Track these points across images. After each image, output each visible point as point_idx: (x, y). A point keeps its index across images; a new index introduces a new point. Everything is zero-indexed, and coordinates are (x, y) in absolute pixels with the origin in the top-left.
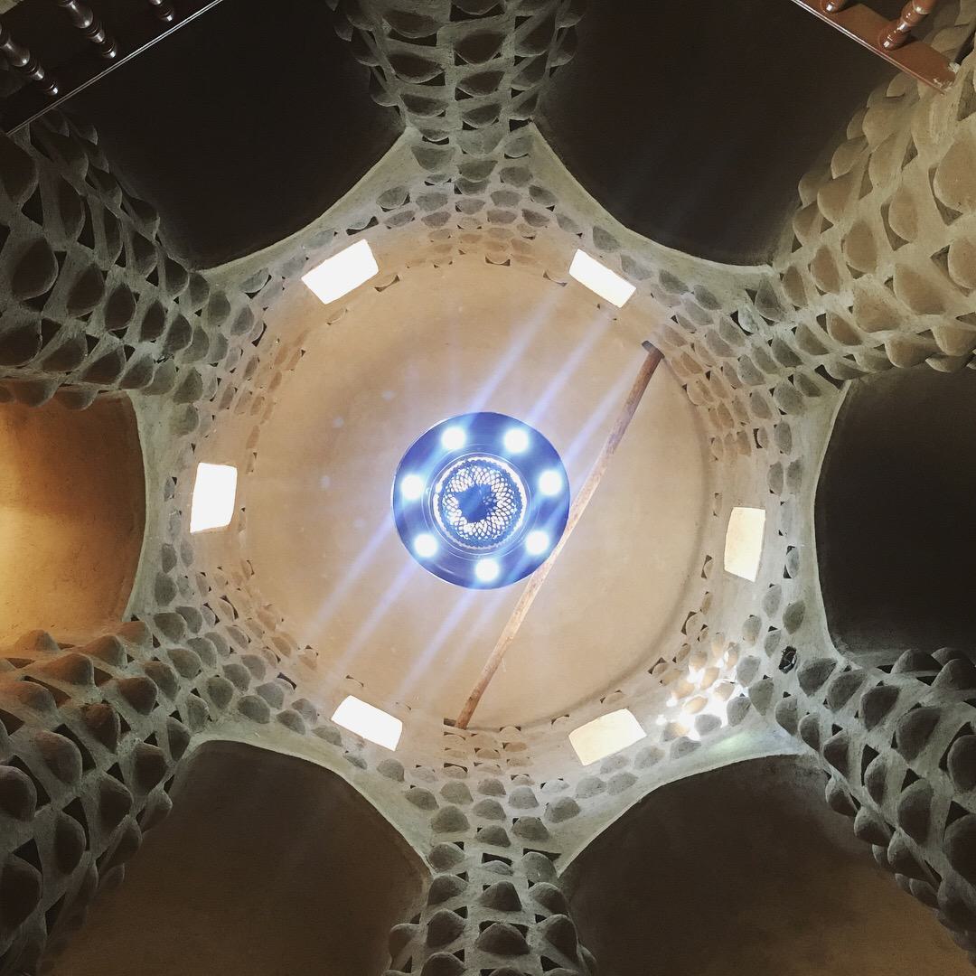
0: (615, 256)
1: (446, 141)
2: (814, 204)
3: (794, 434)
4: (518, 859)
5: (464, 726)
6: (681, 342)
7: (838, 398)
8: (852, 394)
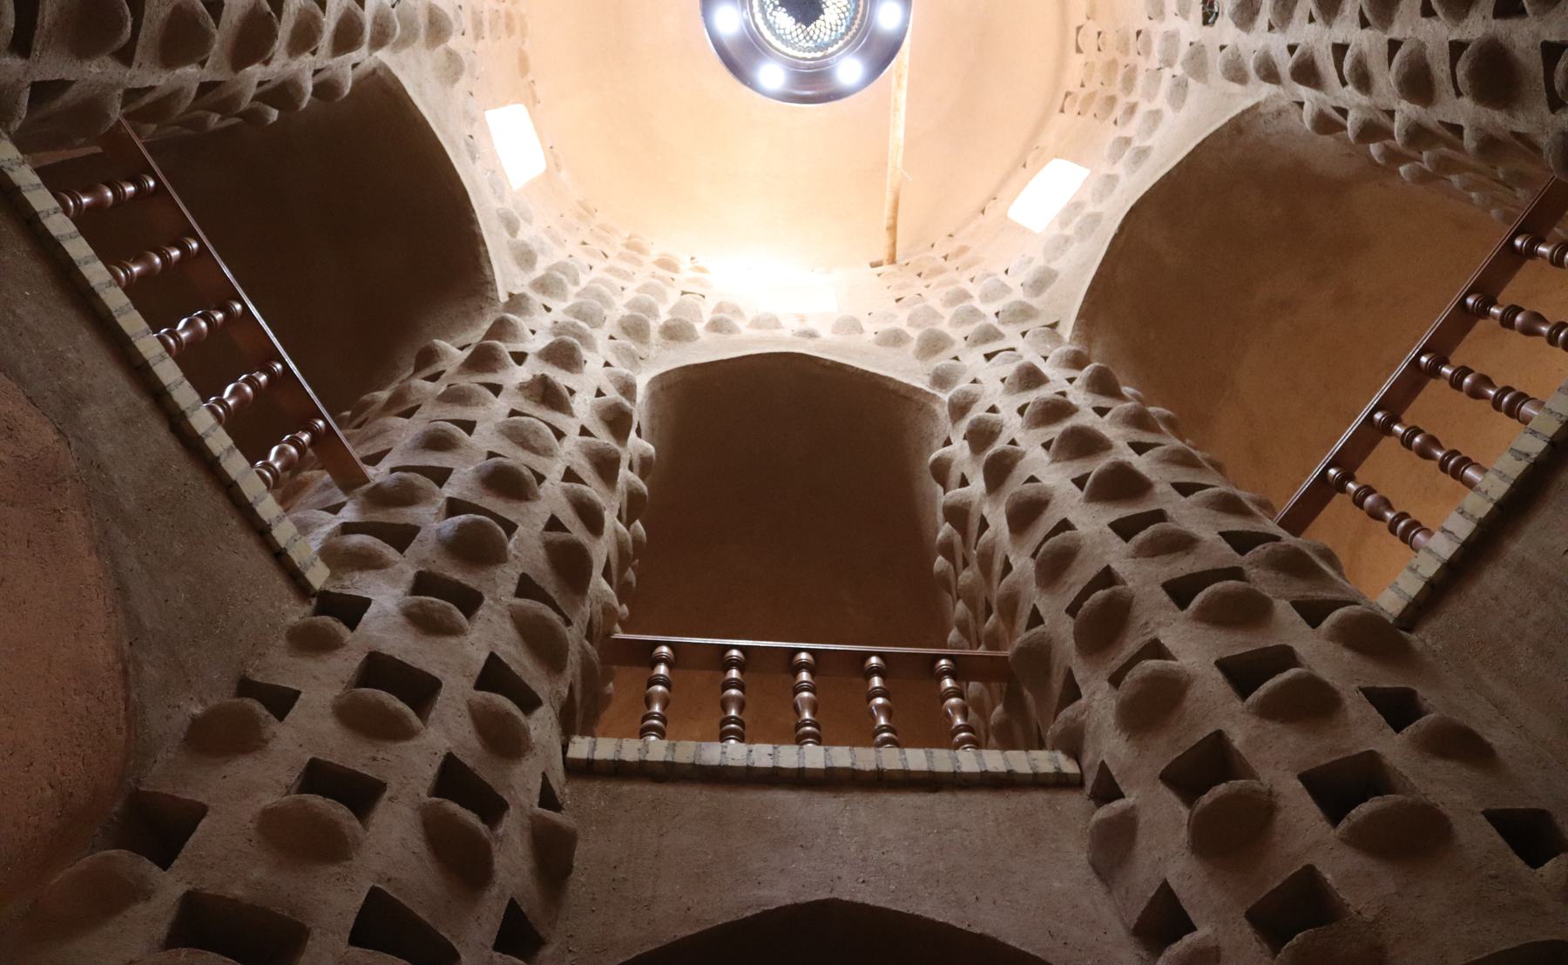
2: (628, 526)
4: (1020, 344)
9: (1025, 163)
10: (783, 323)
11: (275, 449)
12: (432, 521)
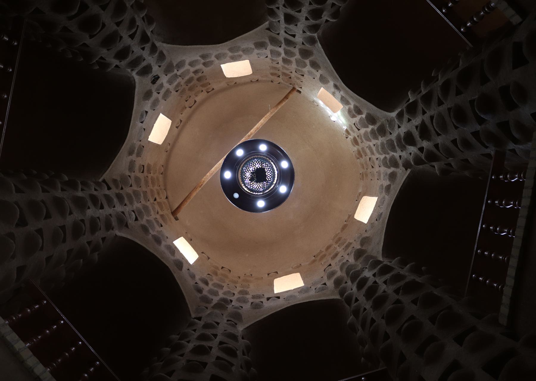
1: (228, 321)
4: (282, 32)
5: (294, 89)
6: (162, 216)
9: (236, 83)
10: (340, 97)
12: (491, 123)
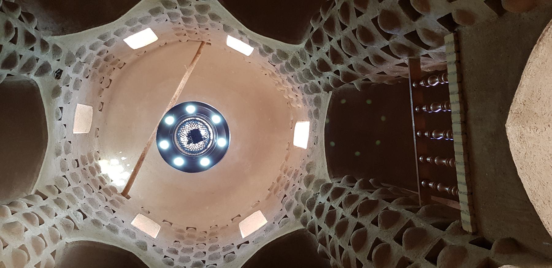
0: (139, 238)
3: (59, 168)
6: (112, 202)
7: (39, 185)
8: (32, 185)
11: (434, 85)
12: (399, 37)
